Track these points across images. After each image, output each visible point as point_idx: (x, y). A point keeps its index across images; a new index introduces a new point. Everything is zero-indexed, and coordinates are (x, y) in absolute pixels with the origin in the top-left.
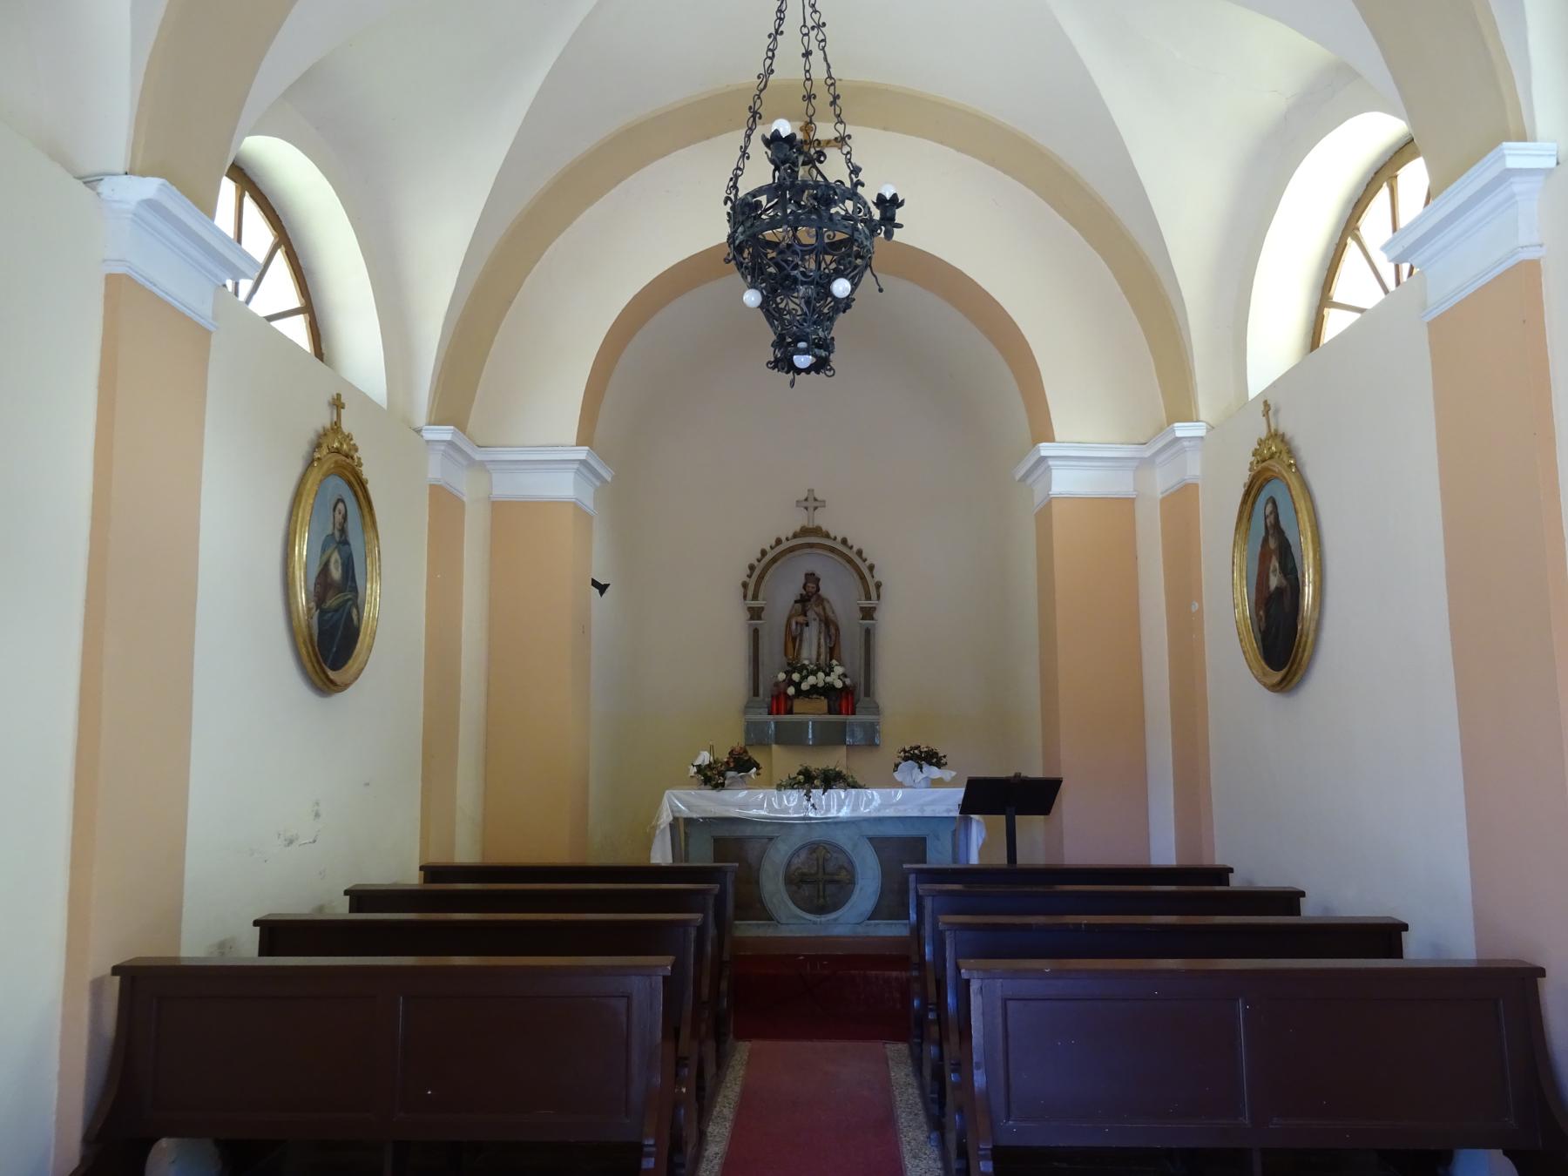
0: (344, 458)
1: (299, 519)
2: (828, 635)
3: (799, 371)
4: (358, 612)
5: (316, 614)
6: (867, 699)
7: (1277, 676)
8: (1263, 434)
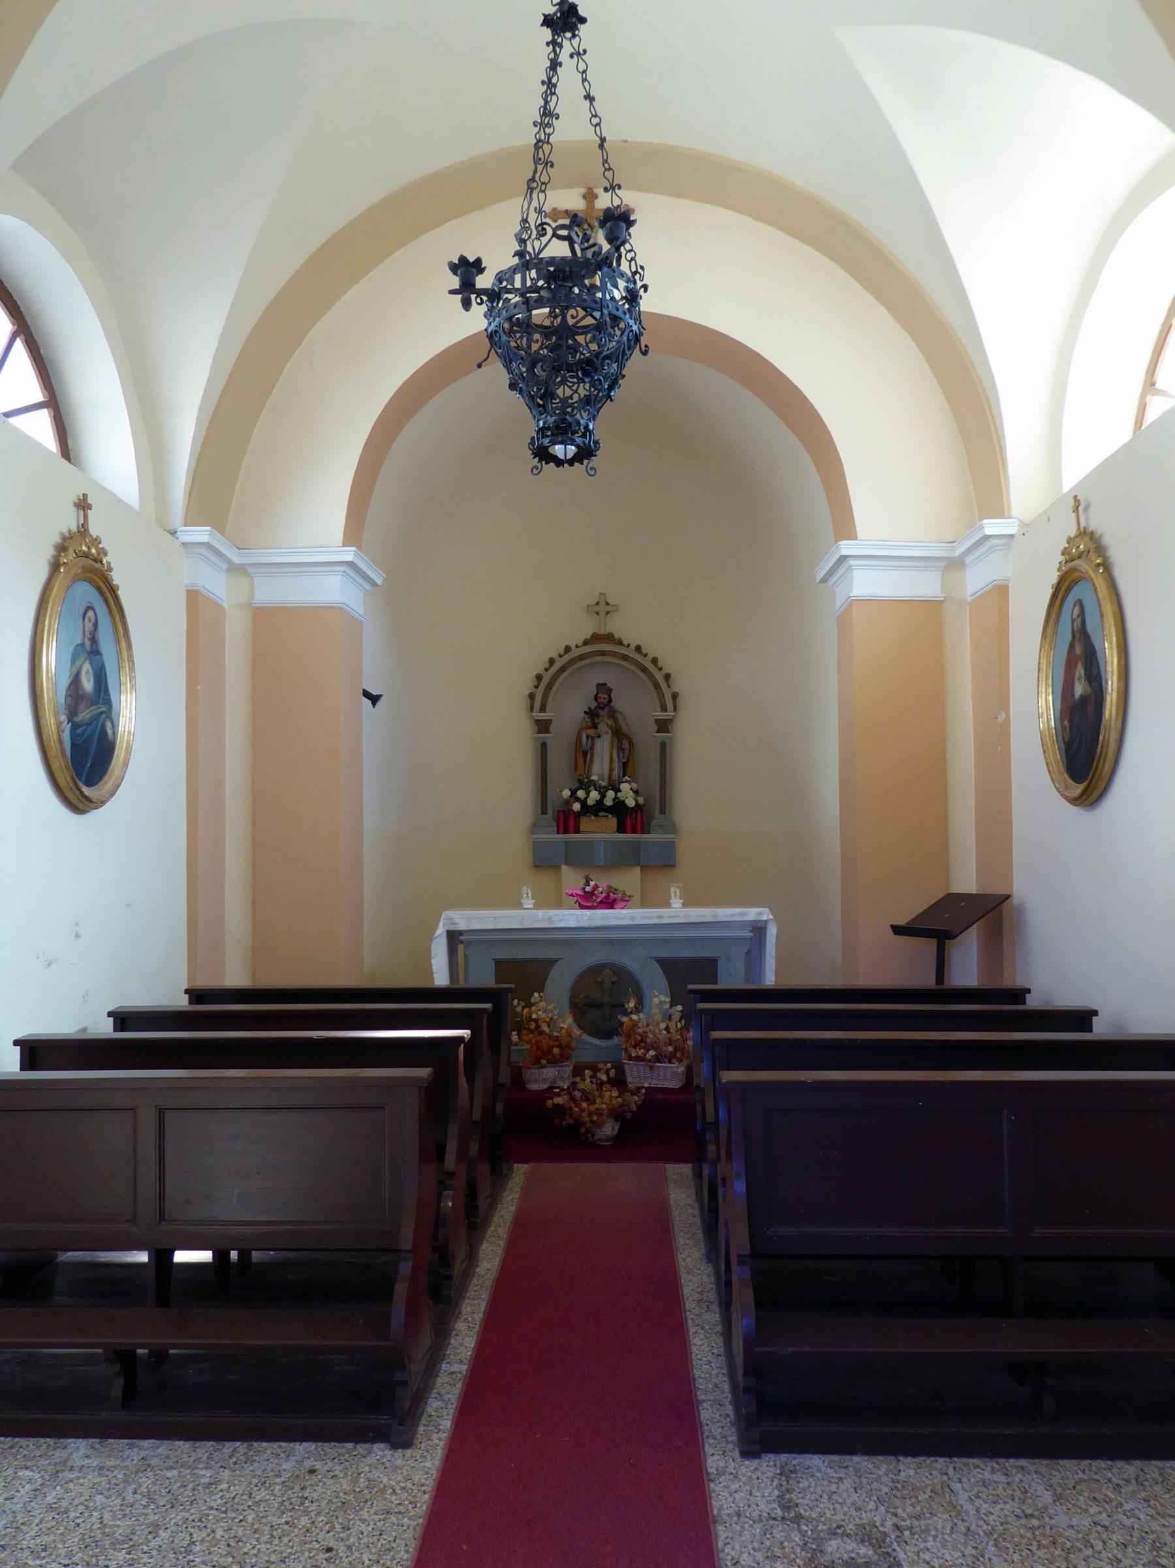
0: (93, 563)
1: (46, 628)
2: (621, 749)
3: (559, 462)
4: (113, 726)
5: (67, 728)
6: (662, 817)
7: (1078, 789)
8: (1073, 532)
